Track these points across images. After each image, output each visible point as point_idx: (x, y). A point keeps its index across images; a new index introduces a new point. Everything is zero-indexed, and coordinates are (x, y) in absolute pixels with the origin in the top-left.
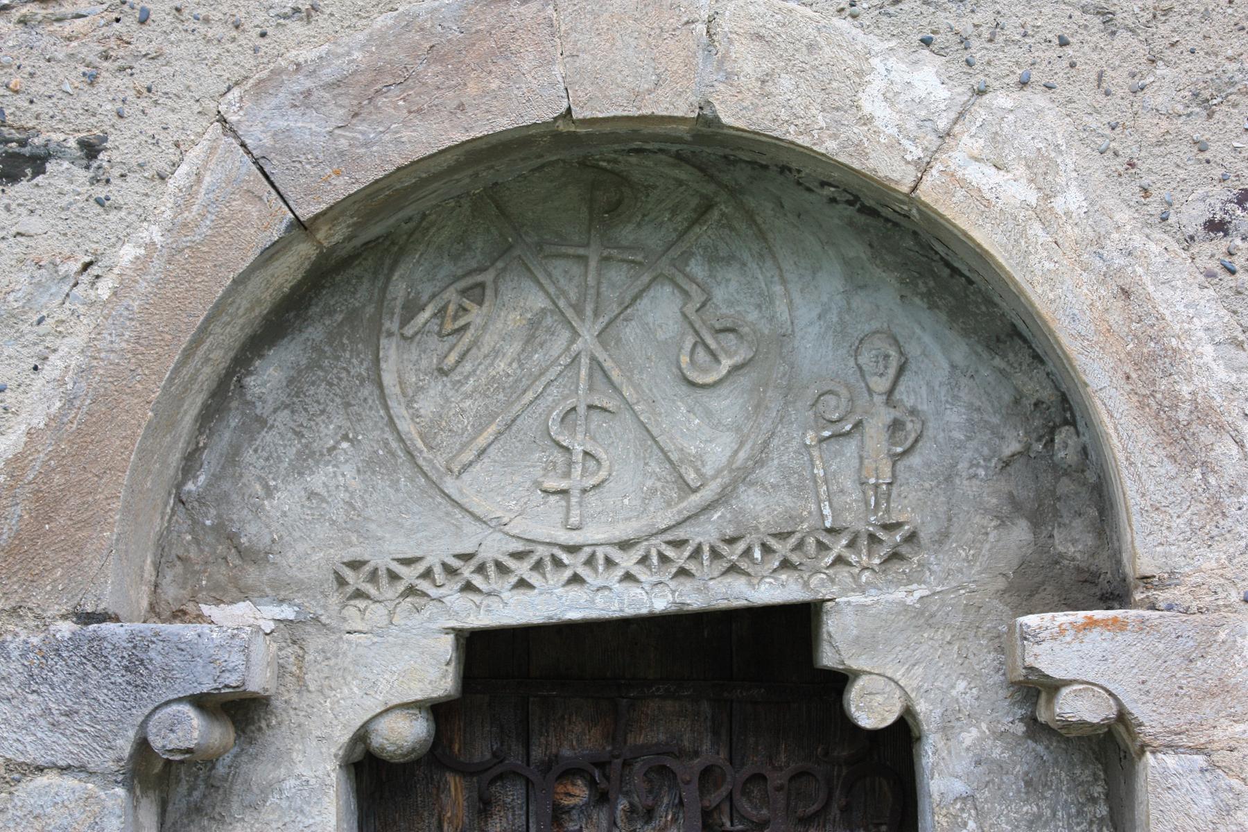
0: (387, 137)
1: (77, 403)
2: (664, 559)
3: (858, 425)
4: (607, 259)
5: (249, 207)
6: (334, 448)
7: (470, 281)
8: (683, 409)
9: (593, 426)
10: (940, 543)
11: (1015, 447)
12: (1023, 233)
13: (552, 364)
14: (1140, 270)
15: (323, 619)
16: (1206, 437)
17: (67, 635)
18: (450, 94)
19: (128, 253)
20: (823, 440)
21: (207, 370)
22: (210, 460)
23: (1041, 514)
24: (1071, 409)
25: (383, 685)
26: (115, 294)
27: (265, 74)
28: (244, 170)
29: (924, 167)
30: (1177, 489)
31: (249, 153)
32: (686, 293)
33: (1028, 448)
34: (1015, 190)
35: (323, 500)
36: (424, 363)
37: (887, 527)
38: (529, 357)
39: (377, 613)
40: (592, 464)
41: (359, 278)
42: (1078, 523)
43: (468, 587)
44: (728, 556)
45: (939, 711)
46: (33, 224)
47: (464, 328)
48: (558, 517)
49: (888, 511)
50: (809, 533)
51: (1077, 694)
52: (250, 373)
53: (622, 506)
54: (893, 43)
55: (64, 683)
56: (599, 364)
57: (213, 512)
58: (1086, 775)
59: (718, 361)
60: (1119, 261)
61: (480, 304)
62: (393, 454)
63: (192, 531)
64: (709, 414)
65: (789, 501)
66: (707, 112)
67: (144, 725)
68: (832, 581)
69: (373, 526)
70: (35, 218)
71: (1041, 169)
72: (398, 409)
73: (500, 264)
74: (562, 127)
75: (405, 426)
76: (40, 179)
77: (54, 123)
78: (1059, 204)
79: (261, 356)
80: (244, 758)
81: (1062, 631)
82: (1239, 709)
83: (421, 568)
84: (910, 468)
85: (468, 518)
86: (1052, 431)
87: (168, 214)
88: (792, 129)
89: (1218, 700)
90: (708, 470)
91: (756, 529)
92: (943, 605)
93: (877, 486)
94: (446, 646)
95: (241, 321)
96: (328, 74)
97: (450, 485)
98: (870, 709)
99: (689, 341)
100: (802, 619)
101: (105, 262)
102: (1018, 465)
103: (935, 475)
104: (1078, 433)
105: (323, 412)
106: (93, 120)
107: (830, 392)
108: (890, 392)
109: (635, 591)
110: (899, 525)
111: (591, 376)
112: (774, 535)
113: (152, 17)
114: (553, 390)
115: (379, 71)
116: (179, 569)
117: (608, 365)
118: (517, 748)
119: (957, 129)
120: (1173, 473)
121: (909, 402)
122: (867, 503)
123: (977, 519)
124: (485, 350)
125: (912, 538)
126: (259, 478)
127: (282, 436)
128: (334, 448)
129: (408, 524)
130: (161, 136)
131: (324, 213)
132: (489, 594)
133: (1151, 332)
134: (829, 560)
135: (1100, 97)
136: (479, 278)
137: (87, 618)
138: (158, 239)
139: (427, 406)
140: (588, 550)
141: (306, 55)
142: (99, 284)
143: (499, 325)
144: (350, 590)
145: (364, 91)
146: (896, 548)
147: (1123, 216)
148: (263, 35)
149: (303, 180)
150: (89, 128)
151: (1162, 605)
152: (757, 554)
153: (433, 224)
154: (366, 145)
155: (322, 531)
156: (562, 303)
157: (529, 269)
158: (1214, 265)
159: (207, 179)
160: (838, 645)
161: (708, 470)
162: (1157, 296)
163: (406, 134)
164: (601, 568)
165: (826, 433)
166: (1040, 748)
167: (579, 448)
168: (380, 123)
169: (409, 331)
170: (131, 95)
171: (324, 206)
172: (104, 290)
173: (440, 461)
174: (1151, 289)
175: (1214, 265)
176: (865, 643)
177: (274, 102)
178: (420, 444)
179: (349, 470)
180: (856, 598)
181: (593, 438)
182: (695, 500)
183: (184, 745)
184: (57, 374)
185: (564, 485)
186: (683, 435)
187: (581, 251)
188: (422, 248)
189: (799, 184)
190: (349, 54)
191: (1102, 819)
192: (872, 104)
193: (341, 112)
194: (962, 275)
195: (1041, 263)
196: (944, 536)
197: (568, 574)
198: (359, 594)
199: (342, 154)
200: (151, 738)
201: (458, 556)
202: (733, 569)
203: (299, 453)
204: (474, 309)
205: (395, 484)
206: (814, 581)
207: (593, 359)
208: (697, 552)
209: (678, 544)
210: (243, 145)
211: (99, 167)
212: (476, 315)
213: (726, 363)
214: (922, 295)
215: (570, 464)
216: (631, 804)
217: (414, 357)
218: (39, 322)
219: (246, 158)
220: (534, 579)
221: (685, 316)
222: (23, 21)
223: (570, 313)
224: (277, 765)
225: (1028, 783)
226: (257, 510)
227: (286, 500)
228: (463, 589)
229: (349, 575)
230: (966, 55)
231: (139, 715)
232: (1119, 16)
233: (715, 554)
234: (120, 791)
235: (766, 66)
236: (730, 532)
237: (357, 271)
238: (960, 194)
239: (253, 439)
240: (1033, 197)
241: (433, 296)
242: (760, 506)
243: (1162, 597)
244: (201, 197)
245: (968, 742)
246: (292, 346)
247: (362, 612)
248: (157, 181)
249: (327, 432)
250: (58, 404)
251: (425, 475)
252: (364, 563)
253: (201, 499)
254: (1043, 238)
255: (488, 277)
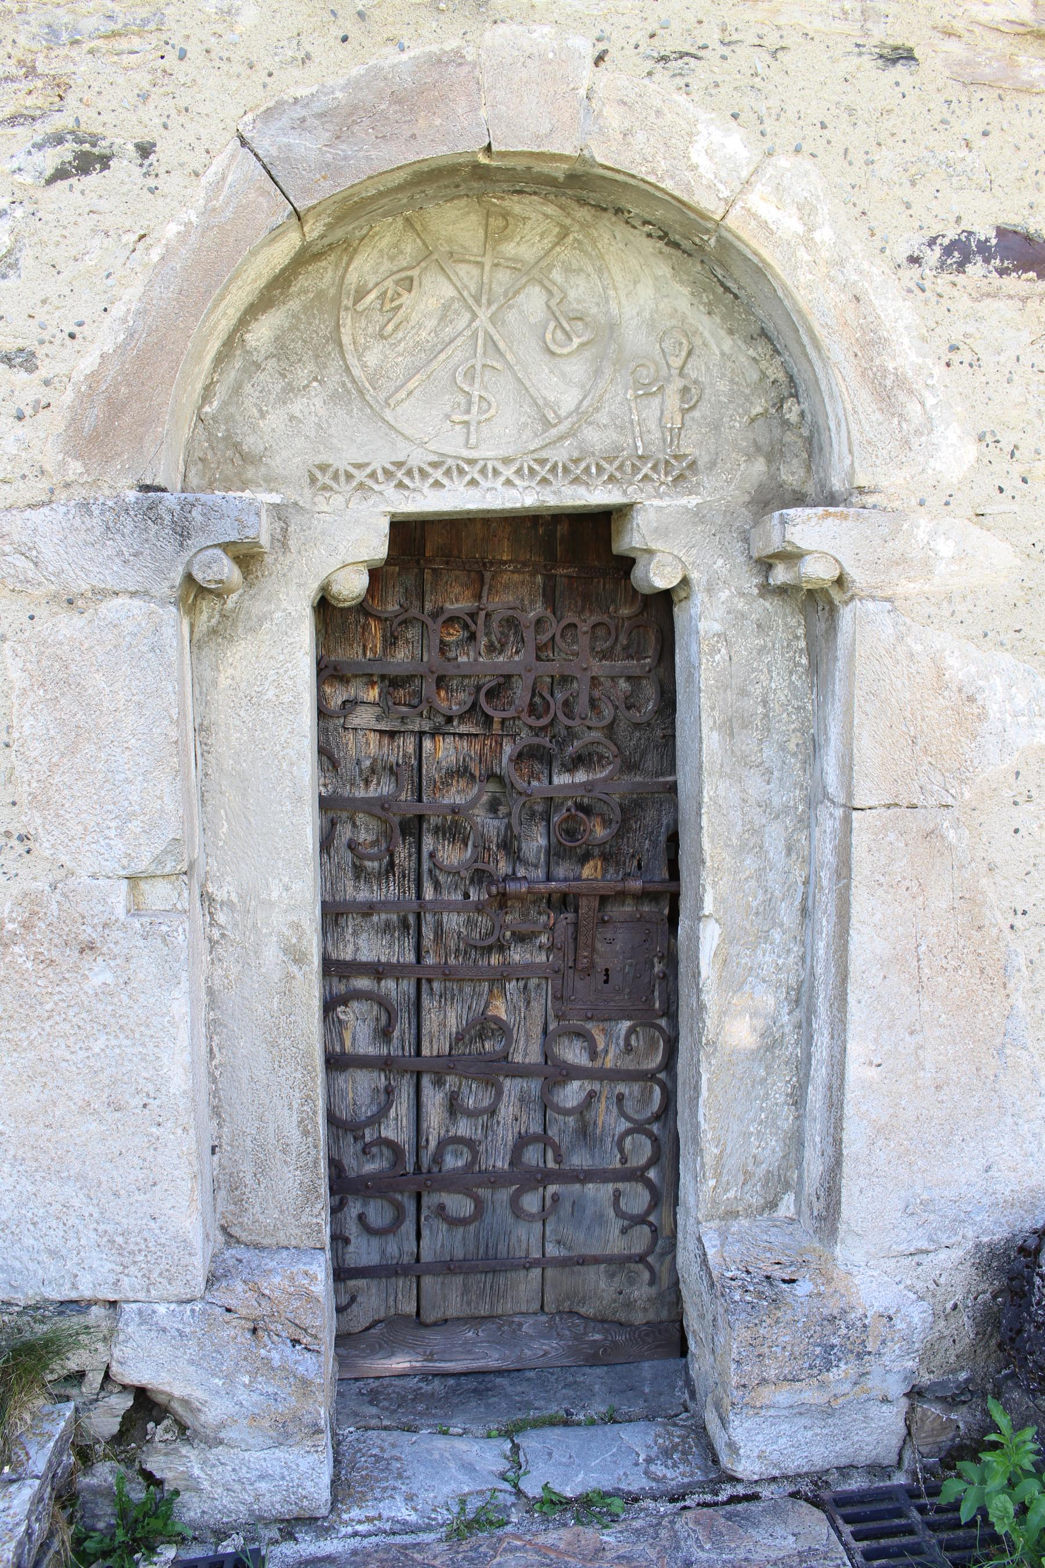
0: (361, 154)
1: (136, 336)
2: (531, 470)
3: (661, 388)
4: (496, 265)
5: (261, 199)
6: (307, 386)
7: (403, 274)
8: (547, 371)
9: (485, 379)
10: (711, 469)
11: (759, 409)
12: (794, 254)
13: (459, 335)
14: (866, 285)
15: (301, 503)
16: (902, 397)
17: (133, 500)
18: (405, 127)
19: (172, 230)
20: (637, 397)
21: (224, 322)
22: (221, 391)
23: (774, 454)
24: (795, 387)
25: (342, 549)
26: (163, 258)
27: (271, 104)
28: (257, 172)
29: (730, 204)
30: (883, 431)
31: (260, 160)
32: (550, 292)
33: (766, 410)
34: (790, 224)
35: (300, 421)
36: (370, 330)
37: (676, 457)
38: (442, 330)
39: (338, 500)
40: (485, 405)
41: (325, 269)
42: (795, 461)
43: (401, 485)
44: (572, 472)
45: (705, 579)
46: (102, 205)
47: (400, 307)
48: (461, 440)
49: (678, 446)
50: (627, 459)
51: (816, 560)
52: (248, 331)
53: (504, 432)
54: (713, 116)
55: (132, 533)
56: (491, 337)
57: (223, 427)
58: (793, 622)
59: (571, 340)
60: (855, 277)
61: (410, 291)
62: (349, 392)
63: (208, 440)
64: (563, 375)
65: (615, 436)
66: (586, 152)
67: (189, 563)
68: (642, 491)
69: (334, 441)
70: (102, 202)
71: (806, 210)
72: (352, 360)
73: (423, 264)
74: (483, 159)
75: (357, 372)
76: (106, 172)
77: (116, 130)
78: (817, 236)
79: (256, 320)
80: (247, 597)
81: (809, 519)
82: (912, 574)
83: (368, 470)
84: (693, 419)
85: (400, 438)
86: (782, 401)
87: (202, 202)
88: (644, 169)
89: (901, 568)
90: (563, 413)
91: (593, 454)
92: (711, 509)
93: (671, 430)
94: (384, 526)
95: (248, 288)
96: (317, 107)
97: (388, 415)
98: (659, 576)
99: (552, 325)
100: (603, 522)
101: (155, 235)
102: (760, 421)
103: (708, 424)
104: (799, 403)
105: (300, 360)
106: (146, 130)
107: (643, 365)
108: (682, 368)
109: (513, 492)
110: (685, 456)
111: (485, 345)
112: (604, 459)
113: (189, 55)
114: (458, 353)
115: (355, 107)
116: (200, 466)
117: (496, 337)
118: (416, 603)
119: (753, 179)
120: (881, 420)
121: (694, 375)
122: (664, 440)
123: (734, 455)
124: (412, 323)
125: (693, 465)
126: (256, 405)
127: (272, 377)
128: (307, 386)
129: (359, 440)
130: (196, 144)
131: (314, 207)
132: (414, 490)
133: (872, 327)
134: (640, 476)
135: (846, 165)
136: (409, 273)
137: (146, 488)
138: (194, 219)
139: (372, 359)
140: (482, 463)
141: (302, 92)
142: (151, 252)
143: (422, 307)
144: (319, 484)
145: (343, 120)
146: (682, 473)
147: (857, 247)
148: (270, 75)
149: (299, 182)
150: (143, 135)
151: (869, 505)
152: (594, 470)
153: (376, 234)
154: (345, 158)
155: (299, 443)
156: (465, 294)
157: (442, 269)
158: (912, 285)
159: (230, 178)
160: (634, 538)
161: (563, 413)
162: (876, 302)
163: (373, 154)
164: (490, 475)
165: (640, 392)
166: (767, 604)
167: (476, 393)
168: (356, 144)
169: (360, 307)
170: (173, 113)
171: (315, 202)
172: (155, 255)
173: (381, 397)
174: (873, 298)
175: (912, 285)
176: (661, 532)
177: (279, 124)
178: (367, 385)
179: (318, 402)
180: (656, 502)
181: (486, 388)
182: (554, 432)
183: (218, 577)
184: (121, 314)
185: (466, 418)
186: (546, 388)
187: (479, 259)
188: (369, 250)
189: (627, 223)
190: (333, 93)
191: (801, 650)
192: (697, 156)
193: (327, 134)
194: (731, 292)
195: (804, 277)
196: (713, 464)
197: (468, 478)
198: (325, 488)
199: (328, 165)
200: (194, 573)
201: (393, 463)
202: (576, 480)
203: (283, 389)
204: (406, 295)
205: (350, 413)
206: (630, 490)
207: (486, 332)
208: (554, 467)
209: (542, 462)
210: (256, 155)
211: (151, 165)
212: (406, 298)
213: (576, 341)
214: (705, 304)
215: (470, 403)
216: (490, 640)
217: (363, 326)
218: (108, 276)
219: (258, 164)
220: (445, 481)
221: (549, 307)
222: (91, 52)
223: (471, 301)
224: (269, 601)
225: (759, 626)
226: (254, 428)
227: (275, 420)
228: (396, 486)
229: (318, 474)
230: (761, 127)
231: (186, 556)
232: (860, 112)
233: (566, 470)
234: (173, 609)
235: (627, 125)
236: (576, 455)
237: (324, 263)
238: (753, 223)
239: (251, 377)
240: (801, 229)
241: (377, 284)
242: (596, 438)
243: (870, 500)
244: (226, 191)
245: (723, 599)
246: (278, 314)
247: (328, 499)
248: (193, 177)
249: (302, 374)
250: (123, 337)
251: (371, 407)
252: (330, 466)
253: (214, 418)
254: (807, 258)
255: (415, 273)
